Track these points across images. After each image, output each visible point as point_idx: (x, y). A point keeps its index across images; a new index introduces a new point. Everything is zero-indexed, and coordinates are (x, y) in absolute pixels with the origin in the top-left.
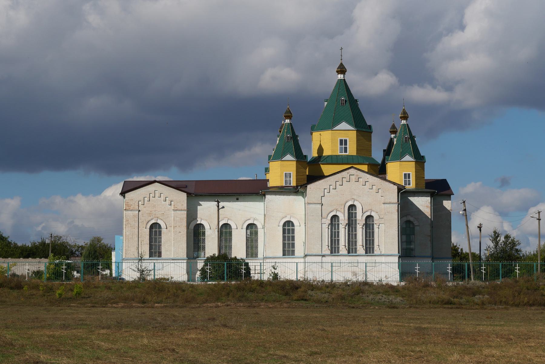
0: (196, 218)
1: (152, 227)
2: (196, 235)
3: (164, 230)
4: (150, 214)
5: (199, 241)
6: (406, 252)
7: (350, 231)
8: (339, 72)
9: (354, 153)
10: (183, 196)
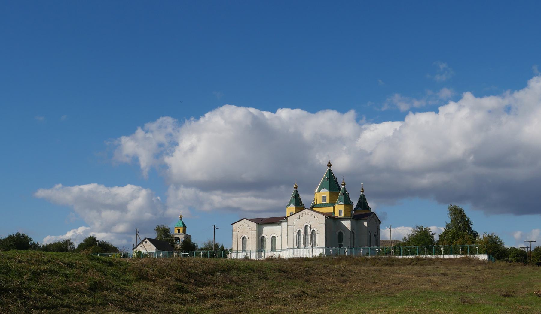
0: (262, 234)
1: (243, 238)
2: (261, 242)
3: (247, 239)
4: (242, 233)
5: (263, 244)
6: (329, 245)
7: (306, 236)
8: (328, 166)
9: (329, 202)
10: (254, 225)
